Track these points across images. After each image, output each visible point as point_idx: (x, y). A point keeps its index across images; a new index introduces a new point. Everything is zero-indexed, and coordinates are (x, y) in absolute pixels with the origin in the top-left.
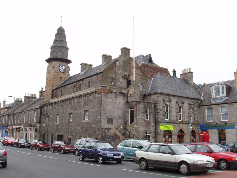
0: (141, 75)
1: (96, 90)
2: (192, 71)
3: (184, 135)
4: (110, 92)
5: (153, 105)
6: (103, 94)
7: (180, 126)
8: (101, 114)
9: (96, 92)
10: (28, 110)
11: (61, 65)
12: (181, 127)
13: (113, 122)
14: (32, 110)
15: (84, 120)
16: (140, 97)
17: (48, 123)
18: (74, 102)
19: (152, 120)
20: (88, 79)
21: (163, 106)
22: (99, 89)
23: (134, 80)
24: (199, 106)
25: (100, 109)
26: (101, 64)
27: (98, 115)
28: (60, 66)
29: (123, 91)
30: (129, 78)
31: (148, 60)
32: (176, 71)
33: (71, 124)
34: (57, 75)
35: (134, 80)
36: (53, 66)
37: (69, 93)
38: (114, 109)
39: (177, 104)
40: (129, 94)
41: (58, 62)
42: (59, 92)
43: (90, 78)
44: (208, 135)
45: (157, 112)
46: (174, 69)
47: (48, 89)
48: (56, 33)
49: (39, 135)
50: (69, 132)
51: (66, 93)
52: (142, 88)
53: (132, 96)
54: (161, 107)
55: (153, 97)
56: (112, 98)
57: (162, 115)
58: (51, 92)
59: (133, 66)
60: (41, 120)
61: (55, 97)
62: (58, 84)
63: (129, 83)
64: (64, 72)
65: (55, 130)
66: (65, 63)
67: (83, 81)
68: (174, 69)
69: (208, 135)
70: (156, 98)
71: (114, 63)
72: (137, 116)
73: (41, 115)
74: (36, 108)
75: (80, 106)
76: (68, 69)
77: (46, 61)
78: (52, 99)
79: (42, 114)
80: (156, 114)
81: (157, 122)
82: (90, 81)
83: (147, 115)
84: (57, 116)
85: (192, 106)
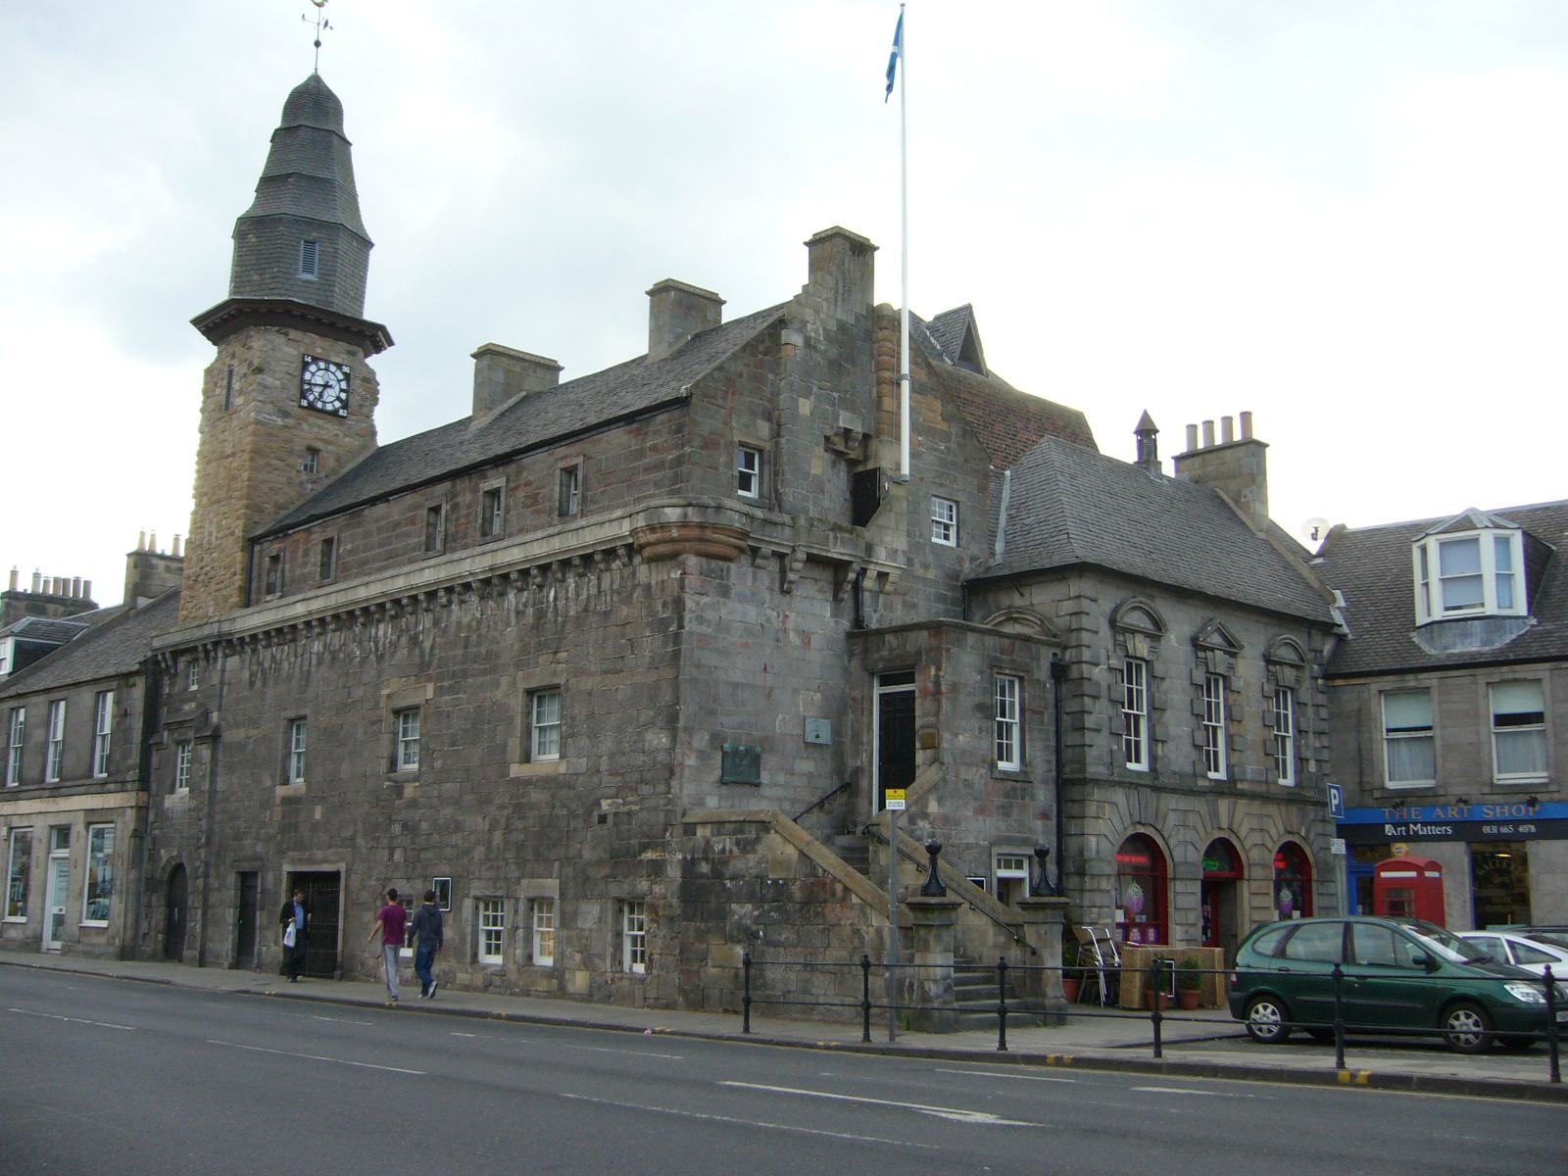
0: (947, 438)
1: (634, 532)
2: (1257, 435)
3: (1241, 878)
4: (741, 550)
5: (1046, 656)
6: (692, 561)
7: (1214, 814)
8: (673, 718)
9: (631, 550)
10: (47, 691)
11: (315, 360)
12: (1225, 825)
13: (765, 777)
14: (72, 692)
15: (527, 758)
16: (942, 599)
17: (213, 782)
18: (436, 622)
19: (1042, 764)
20: (561, 451)
21: (1111, 669)
22: (664, 527)
23: (906, 470)
24: (1327, 677)
25: (669, 674)
26: (467, 411)
27: (651, 724)
28: (305, 366)
29: (836, 552)
30: (866, 458)
31: (957, 347)
32: (1156, 431)
33: (409, 791)
34: (286, 434)
35: (906, 470)
36: (256, 362)
37: (392, 559)
38: (770, 680)
39: (1201, 654)
40: (872, 573)
41: (294, 334)
42: (306, 553)
43: (578, 447)
44: (1438, 882)
45: (1072, 706)
46: (1146, 419)
47: (214, 529)
48: (277, 123)
49: (133, 874)
50: (392, 850)
51: (363, 563)
52: (953, 533)
53: (888, 587)
54: (1099, 674)
55: (1042, 598)
56: (754, 598)
57: (1105, 732)
58: (239, 557)
59: (899, 371)
60: (155, 760)
61: (270, 590)
62: (289, 488)
63: (866, 497)
64: (334, 413)
65: (269, 839)
66: (342, 346)
67: (519, 473)
68: (1146, 419)
69: (1438, 882)
70: (1068, 606)
71: (768, 343)
72: (946, 736)
73: (151, 726)
74: (110, 671)
75: (491, 656)
76: (364, 392)
77: (197, 322)
78: (247, 604)
79: (165, 716)
80: (1066, 719)
81: (1073, 782)
82: (571, 471)
83: (1003, 730)
84: (288, 732)
85: (1288, 675)
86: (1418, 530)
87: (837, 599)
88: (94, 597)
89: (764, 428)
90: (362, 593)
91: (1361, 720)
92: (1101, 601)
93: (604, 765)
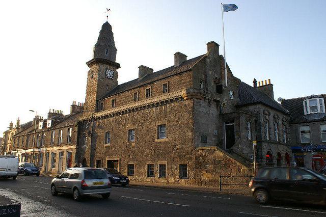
24: (289, 124)
26: (173, 64)
29: (218, 99)
33: (133, 144)
37: (126, 103)
46: (255, 79)
55: (251, 108)
68: (255, 79)
76: (116, 75)
86: (305, 98)
87: (217, 108)
88: (63, 114)
89: (203, 76)
90: (122, 109)
91: (297, 130)
92: (262, 108)
93: (177, 139)
